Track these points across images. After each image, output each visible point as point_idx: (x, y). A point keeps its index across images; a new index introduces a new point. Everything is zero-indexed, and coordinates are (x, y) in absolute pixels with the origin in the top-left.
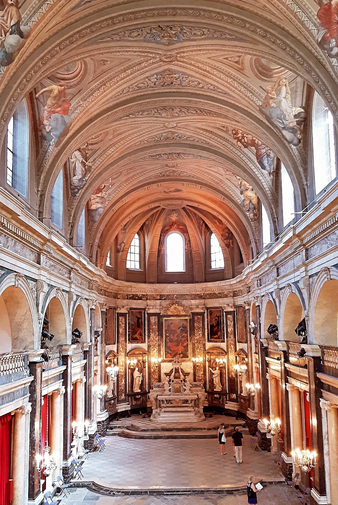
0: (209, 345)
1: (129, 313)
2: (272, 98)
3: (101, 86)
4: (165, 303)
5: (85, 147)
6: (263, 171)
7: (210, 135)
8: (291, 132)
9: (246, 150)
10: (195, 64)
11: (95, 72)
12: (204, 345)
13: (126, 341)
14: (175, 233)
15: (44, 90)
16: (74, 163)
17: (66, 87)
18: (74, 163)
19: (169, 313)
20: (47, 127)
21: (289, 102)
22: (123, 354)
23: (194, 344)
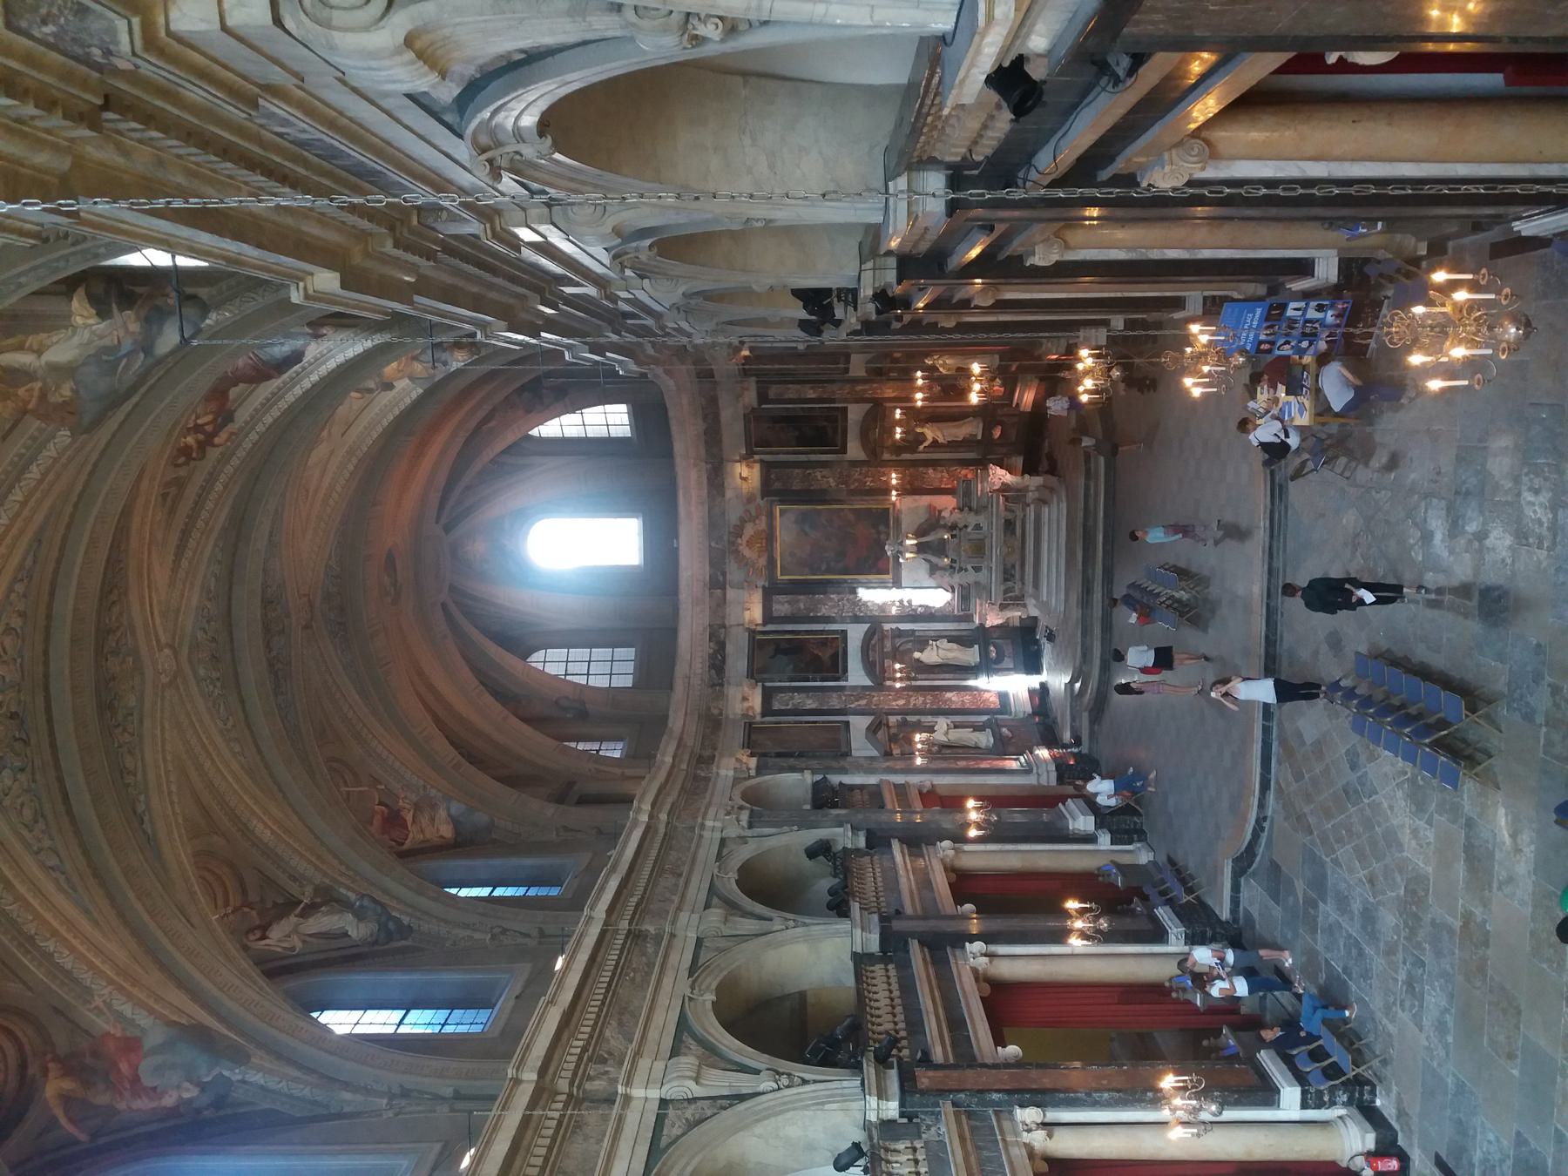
0: (855, 450)
1: (763, 681)
2: (43, 395)
4: (734, 572)
5: (254, 913)
6: (308, 357)
7: (195, 535)
8: (160, 328)
9: (242, 415)
12: (854, 463)
13: (842, 688)
14: (525, 539)
15: (63, 1121)
16: (308, 939)
18: (308, 939)
19: (763, 561)
20: (186, 1095)
21: (55, 339)
22: (877, 698)
23: (853, 493)
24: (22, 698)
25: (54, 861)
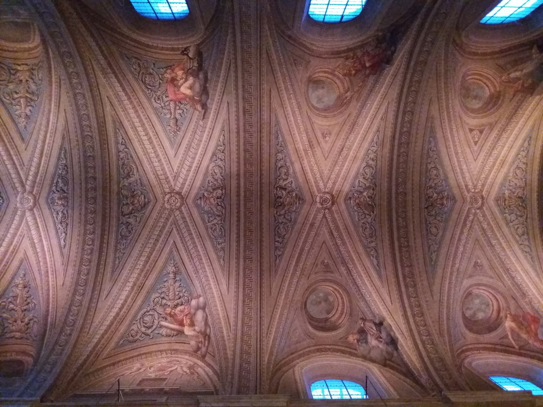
3: (510, 274)
10: (486, 173)
11: (491, 277)
15: (510, 337)
17: (508, 312)
24: (525, 193)
25: (527, 249)
